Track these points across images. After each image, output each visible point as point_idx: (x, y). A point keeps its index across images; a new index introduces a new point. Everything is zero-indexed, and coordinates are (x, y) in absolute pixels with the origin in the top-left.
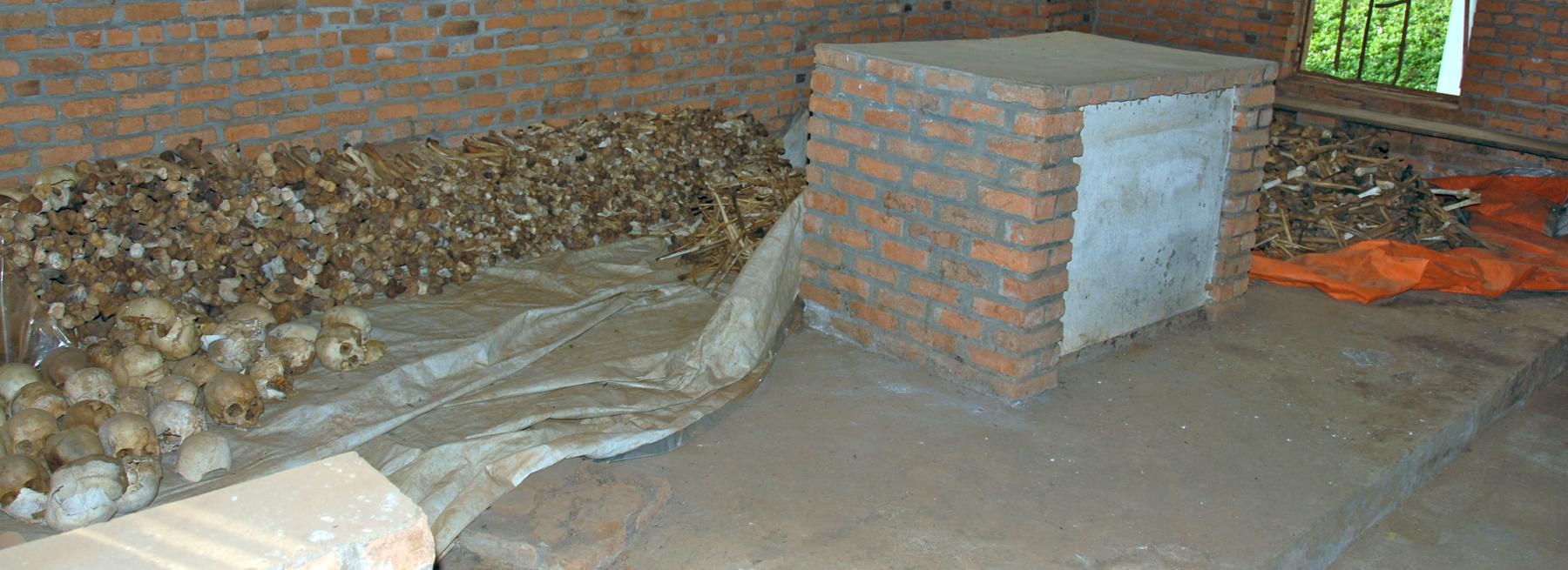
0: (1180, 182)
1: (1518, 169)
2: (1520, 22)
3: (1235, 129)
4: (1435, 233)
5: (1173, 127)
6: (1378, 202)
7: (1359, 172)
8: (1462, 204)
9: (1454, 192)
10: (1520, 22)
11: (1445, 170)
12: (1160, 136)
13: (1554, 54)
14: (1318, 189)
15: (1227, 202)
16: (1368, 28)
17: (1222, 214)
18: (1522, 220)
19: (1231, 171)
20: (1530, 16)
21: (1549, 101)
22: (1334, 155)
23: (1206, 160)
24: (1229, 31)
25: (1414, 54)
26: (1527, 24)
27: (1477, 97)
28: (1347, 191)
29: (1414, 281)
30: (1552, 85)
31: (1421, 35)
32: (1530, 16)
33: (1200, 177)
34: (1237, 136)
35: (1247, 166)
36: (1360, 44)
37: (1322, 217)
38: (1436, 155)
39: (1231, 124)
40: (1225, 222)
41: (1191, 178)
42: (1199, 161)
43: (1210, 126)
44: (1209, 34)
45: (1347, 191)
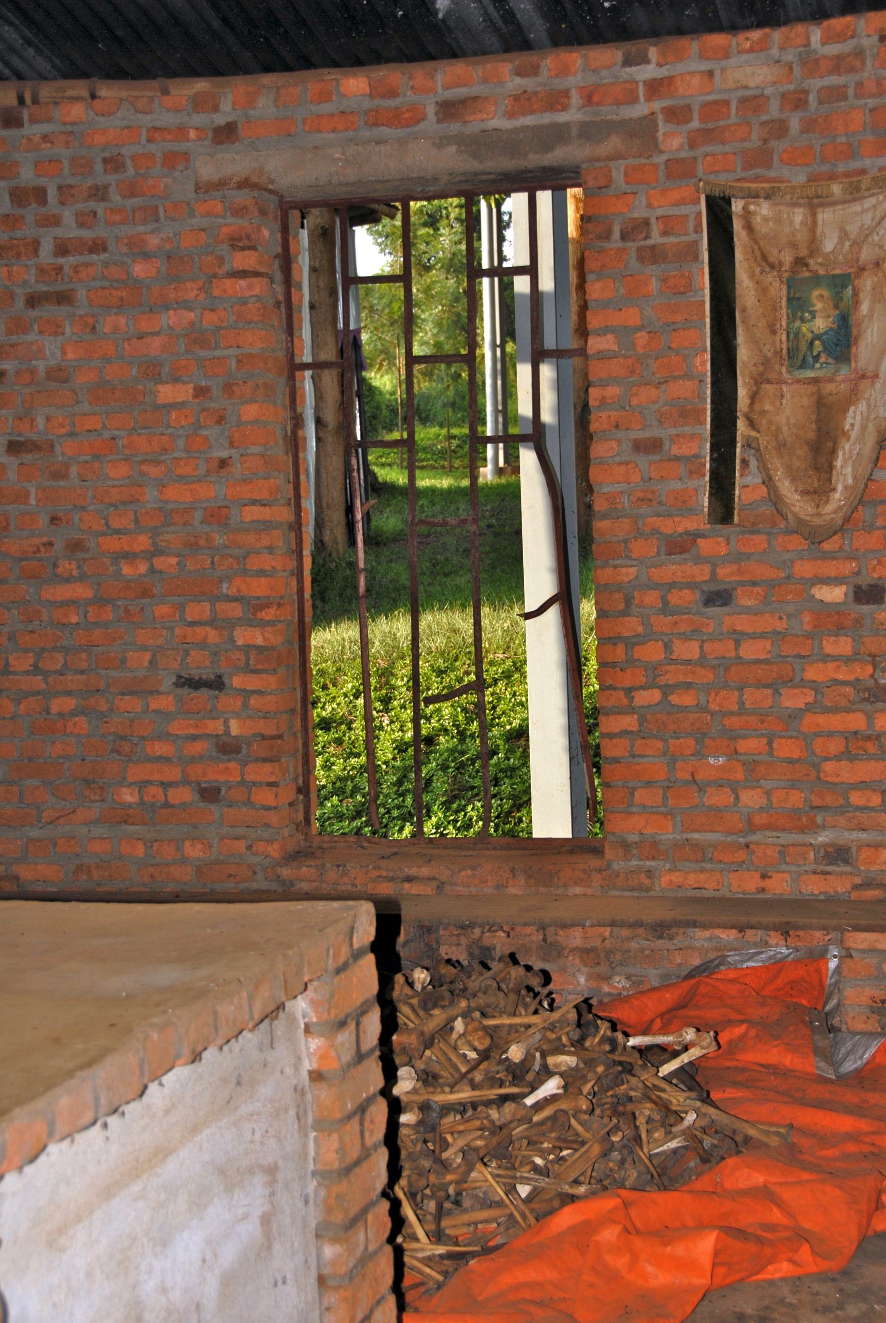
0: (229, 1254)
1: (733, 957)
2: (674, 699)
3: (316, 1076)
4: (669, 1135)
5: (195, 1129)
6: (563, 1105)
7: (515, 1053)
8: (685, 1058)
9: (661, 1039)
10: (674, 699)
11: (607, 979)
12: (171, 1167)
13: (743, 746)
14: (446, 1109)
15: (329, 1251)
16: (368, 718)
17: (322, 1280)
18: (775, 1054)
19: (323, 1175)
20: (688, 686)
21: (752, 828)
22: (459, 1025)
23: (271, 1171)
24: (165, 785)
25: (452, 751)
26: (687, 699)
27: (633, 838)
28: (504, 1099)
29: (701, 1281)
30: (751, 799)
31: (454, 717)
32: (688, 686)
33: (266, 1220)
34: (324, 1093)
35: (354, 1152)
36: (361, 747)
37: (471, 1168)
38: (587, 953)
39: (307, 1065)
40: (331, 1298)
41: (250, 1229)
42: (259, 1180)
43: (265, 1091)
44: (129, 797)
45: (504, 1099)
